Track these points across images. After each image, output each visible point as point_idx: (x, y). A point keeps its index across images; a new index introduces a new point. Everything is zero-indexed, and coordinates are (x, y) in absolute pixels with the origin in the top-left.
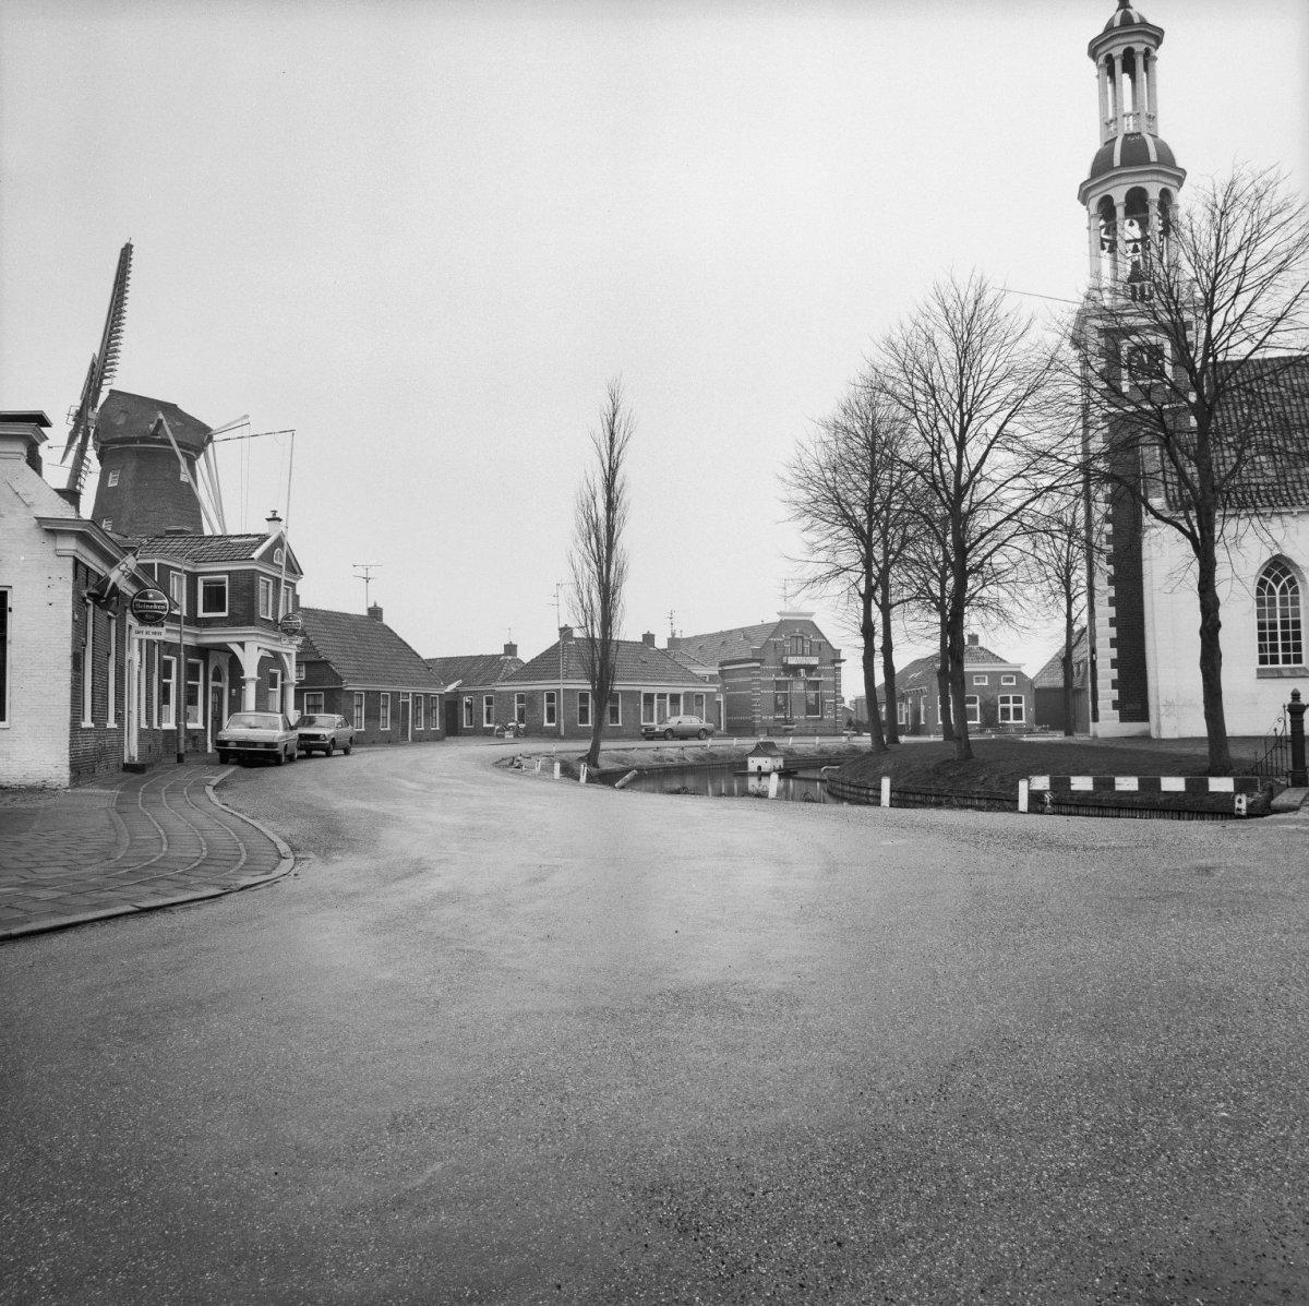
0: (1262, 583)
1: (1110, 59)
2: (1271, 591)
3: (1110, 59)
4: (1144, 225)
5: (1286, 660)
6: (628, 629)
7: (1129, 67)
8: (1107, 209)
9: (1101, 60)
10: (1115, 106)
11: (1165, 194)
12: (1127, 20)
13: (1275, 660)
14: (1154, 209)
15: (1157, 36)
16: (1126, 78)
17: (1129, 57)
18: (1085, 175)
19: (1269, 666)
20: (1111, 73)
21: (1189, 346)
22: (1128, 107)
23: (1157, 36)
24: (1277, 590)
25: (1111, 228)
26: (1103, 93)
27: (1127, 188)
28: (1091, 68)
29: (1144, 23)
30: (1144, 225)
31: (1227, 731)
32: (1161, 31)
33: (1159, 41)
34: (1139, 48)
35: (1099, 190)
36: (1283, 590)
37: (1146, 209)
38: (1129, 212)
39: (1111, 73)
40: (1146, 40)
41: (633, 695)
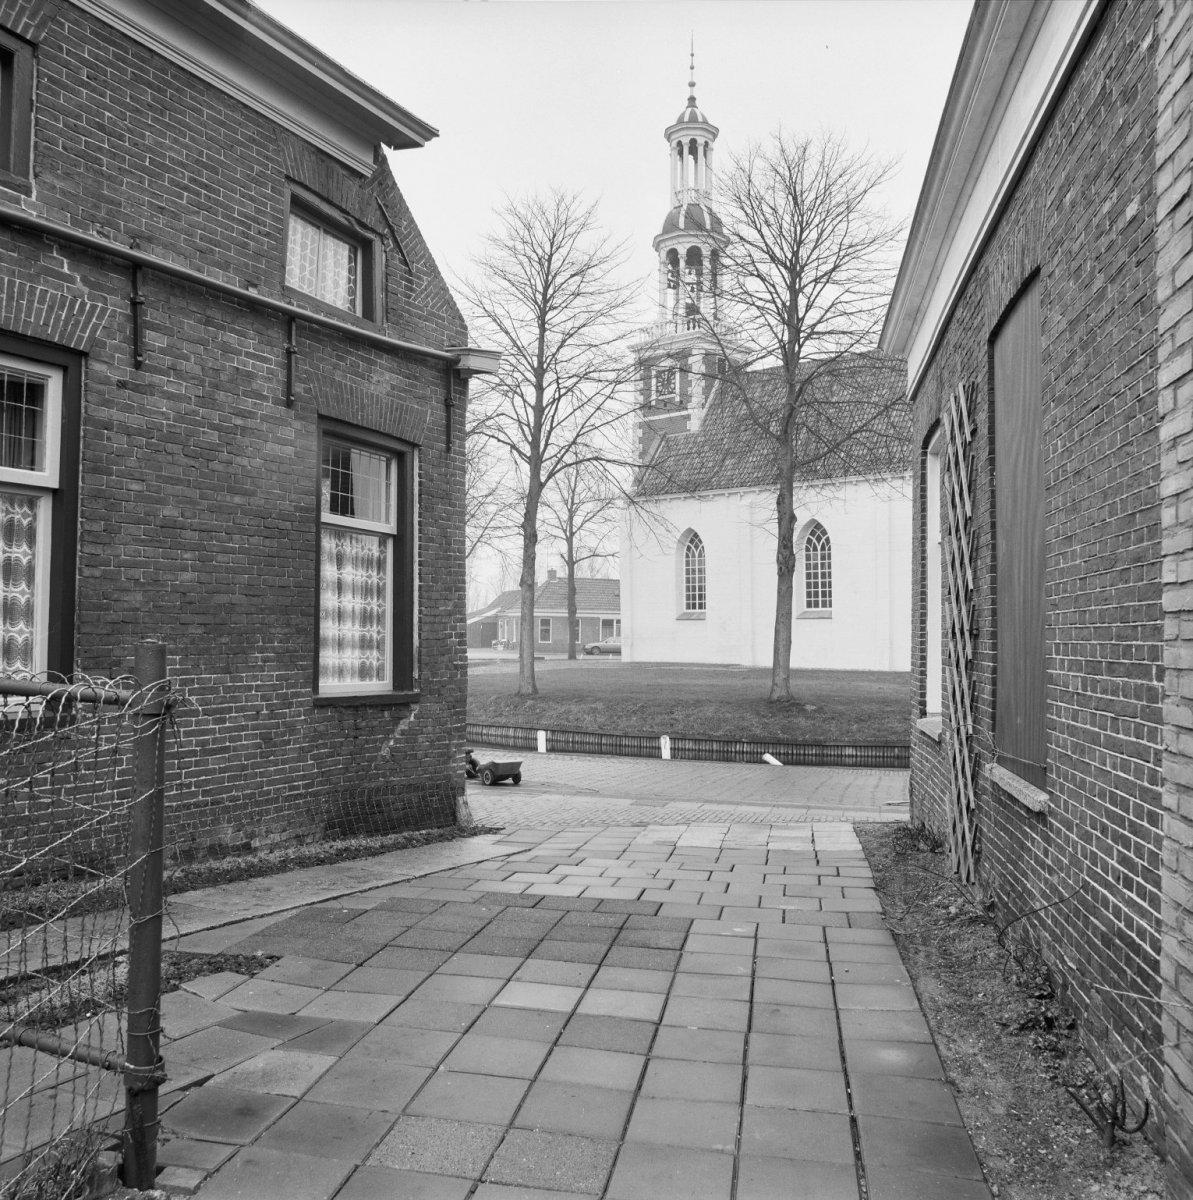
0: (809, 541)
1: (680, 144)
2: (815, 549)
3: (680, 144)
4: (699, 274)
5: (824, 605)
6: (795, 662)
7: (693, 151)
8: (673, 256)
9: (674, 143)
10: (682, 178)
11: (706, 144)
12: (693, 118)
13: (817, 605)
14: (707, 264)
15: (714, 133)
16: (691, 157)
17: (693, 142)
18: (659, 230)
19: (813, 609)
20: (681, 153)
21: (382, 847)
22: (692, 184)
23: (714, 133)
24: (819, 548)
25: (676, 273)
26: (674, 169)
27: (690, 245)
28: (666, 149)
29: (705, 122)
30: (699, 274)
31: (746, 660)
32: (717, 130)
33: (715, 136)
34: (701, 141)
35: (692, 239)
36: (823, 548)
37: (701, 263)
38: (689, 263)
39: (681, 153)
40: (706, 134)
41: (594, 621)
